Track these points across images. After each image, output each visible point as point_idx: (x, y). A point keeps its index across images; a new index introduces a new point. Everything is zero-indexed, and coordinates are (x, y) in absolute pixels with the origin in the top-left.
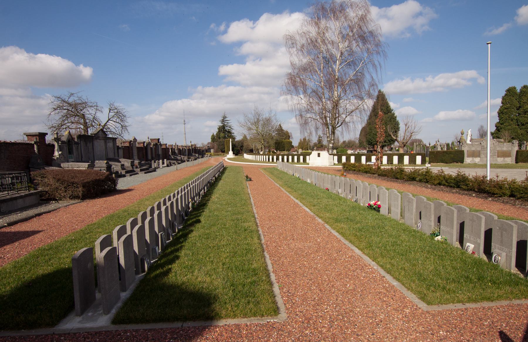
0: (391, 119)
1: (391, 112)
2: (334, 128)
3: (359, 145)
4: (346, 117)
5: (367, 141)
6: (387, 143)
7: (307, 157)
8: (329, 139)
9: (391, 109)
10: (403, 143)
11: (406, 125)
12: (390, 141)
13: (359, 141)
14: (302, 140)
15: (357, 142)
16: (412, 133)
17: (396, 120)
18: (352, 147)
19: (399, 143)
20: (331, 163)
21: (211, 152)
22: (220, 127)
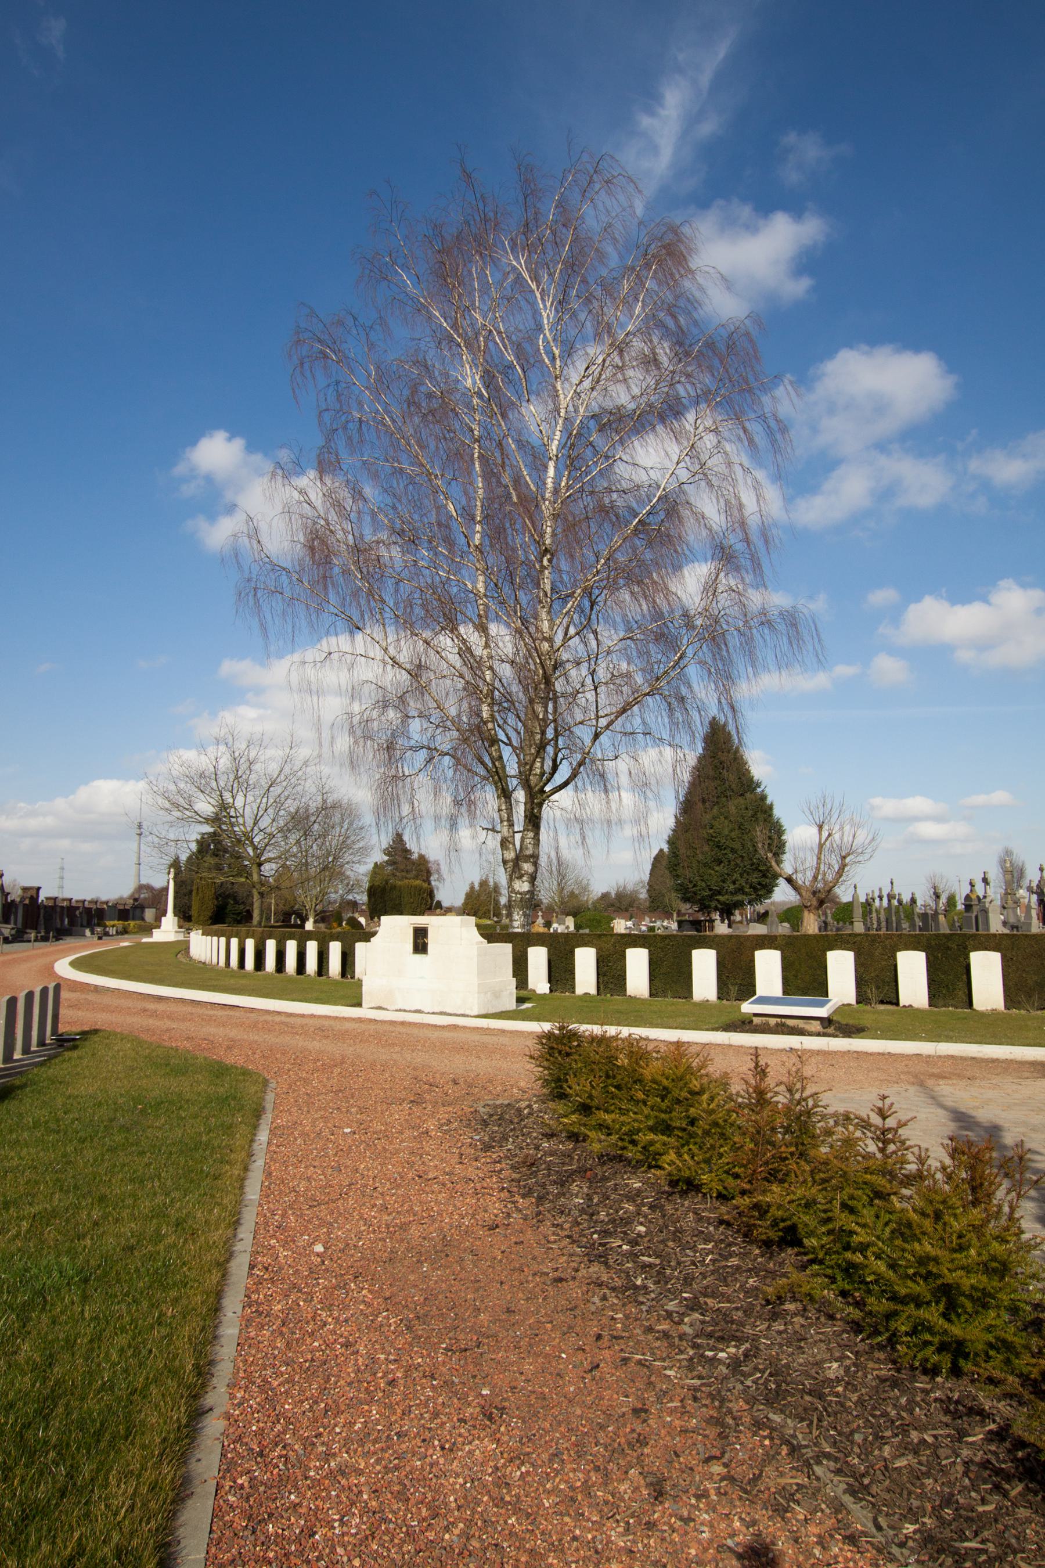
0: (756, 814)
1: (755, 789)
2: (537, 798)
3: (647, 904)
4: (597, 736)
5: (679, 887)
6: (746, 894)
7: (360, 947)
8: (510, 855)
9: (755, 778)
10: (814, 893)
11: (820, 827)
12: (755, 889)
13: (648, 891)
14: (477, 887)
15: (643, 895)
16: (844, 858)
17: (771, 815)
18: (627, 910)
19: (800, 894)
20: (497, 995)
21: (143, 919)
22: (203, 838)
